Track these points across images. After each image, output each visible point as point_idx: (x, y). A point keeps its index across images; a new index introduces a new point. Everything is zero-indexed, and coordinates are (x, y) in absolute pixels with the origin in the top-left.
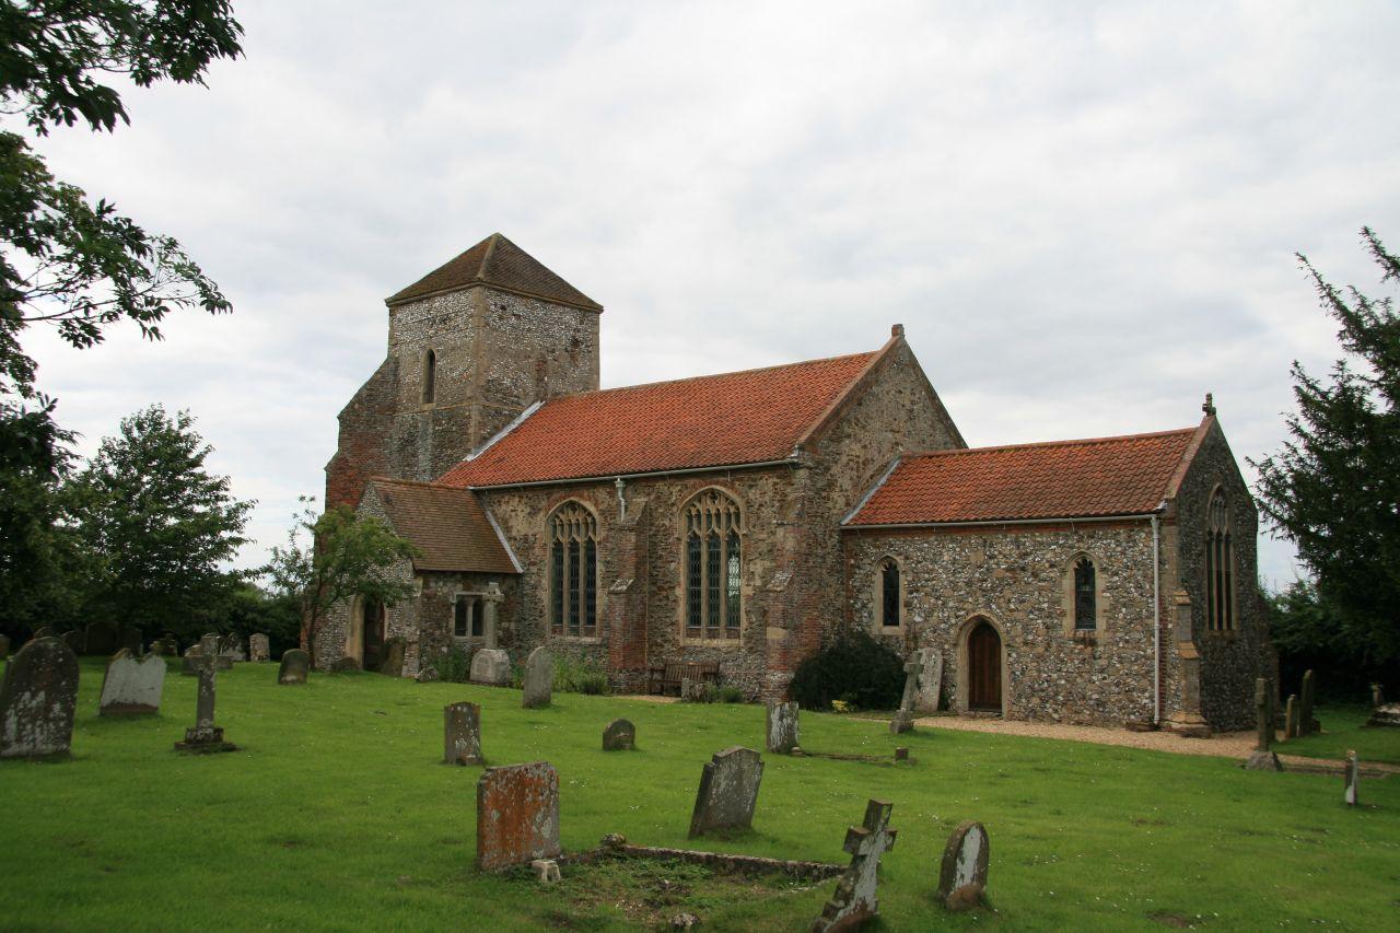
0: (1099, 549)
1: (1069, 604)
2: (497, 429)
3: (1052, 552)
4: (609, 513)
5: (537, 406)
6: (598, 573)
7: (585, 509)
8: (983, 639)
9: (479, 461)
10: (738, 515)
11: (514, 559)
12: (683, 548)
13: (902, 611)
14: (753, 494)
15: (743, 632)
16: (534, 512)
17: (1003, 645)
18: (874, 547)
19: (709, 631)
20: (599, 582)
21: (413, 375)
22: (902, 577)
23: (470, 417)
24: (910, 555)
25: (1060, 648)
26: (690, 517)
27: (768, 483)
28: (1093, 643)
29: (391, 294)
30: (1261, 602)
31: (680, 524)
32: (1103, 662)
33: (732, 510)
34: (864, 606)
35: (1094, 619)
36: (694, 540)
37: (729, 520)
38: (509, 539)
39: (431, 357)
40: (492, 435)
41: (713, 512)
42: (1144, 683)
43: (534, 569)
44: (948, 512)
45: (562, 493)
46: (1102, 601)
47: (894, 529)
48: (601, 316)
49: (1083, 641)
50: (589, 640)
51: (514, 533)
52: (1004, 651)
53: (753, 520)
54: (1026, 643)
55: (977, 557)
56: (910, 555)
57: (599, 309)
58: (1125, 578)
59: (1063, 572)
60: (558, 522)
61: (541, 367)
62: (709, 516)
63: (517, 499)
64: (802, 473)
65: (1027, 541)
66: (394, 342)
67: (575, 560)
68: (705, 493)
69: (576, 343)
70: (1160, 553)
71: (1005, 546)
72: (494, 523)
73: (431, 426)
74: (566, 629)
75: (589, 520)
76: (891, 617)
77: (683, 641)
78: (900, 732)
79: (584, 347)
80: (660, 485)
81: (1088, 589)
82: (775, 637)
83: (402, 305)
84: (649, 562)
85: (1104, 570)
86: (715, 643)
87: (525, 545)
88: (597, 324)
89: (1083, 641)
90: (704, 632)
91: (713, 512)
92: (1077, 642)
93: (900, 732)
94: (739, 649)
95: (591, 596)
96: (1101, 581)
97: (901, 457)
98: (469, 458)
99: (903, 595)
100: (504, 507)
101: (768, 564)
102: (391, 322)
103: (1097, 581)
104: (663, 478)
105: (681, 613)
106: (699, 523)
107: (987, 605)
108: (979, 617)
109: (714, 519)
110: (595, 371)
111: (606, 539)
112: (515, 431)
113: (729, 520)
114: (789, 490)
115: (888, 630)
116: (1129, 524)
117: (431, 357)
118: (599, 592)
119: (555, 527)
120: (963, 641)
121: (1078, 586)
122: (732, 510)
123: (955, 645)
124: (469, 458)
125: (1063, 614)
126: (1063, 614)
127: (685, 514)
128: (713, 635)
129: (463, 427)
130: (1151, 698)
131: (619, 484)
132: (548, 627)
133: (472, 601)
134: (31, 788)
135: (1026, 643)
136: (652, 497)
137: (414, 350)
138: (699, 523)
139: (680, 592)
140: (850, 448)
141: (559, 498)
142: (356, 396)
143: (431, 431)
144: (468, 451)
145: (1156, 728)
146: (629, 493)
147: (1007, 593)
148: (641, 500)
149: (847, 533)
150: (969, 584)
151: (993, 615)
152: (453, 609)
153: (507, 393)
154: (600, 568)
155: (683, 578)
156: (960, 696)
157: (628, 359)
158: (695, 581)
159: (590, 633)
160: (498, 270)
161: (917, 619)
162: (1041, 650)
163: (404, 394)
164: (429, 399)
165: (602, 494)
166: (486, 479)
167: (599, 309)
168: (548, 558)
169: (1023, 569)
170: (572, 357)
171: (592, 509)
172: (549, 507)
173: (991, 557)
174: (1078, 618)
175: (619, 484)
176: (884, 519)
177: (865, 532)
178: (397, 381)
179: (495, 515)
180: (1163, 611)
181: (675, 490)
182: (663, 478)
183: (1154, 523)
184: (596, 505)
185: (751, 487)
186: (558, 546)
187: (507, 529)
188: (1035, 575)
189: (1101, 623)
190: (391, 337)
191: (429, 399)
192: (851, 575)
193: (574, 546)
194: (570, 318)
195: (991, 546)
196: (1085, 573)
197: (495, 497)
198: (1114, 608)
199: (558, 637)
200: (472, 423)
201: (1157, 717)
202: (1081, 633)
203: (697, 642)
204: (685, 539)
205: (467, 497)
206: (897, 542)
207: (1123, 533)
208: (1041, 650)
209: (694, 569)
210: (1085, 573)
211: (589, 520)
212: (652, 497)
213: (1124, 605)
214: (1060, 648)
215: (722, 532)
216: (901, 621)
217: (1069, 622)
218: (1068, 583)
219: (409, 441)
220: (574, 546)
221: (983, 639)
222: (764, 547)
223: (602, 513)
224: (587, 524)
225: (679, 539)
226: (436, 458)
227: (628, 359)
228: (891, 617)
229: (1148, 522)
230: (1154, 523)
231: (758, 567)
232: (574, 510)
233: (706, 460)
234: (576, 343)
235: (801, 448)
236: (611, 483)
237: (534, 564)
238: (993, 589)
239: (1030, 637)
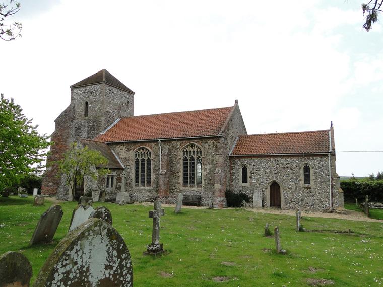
0: (311, 162)
1: (302, 177)
2: (108, 126)
3: (297, 162)
4: (155, 151)
5: (119, 119)
6: (152, 168)
7: (147, 149)
8: (275, 188)
9: (105, 134)
10: (201, 151)
11: (122, 164)
12: (182, 161)
13: (249, 179)
14: (205, 145)
15: (202, 185)
16: (129, 150)
17: (281, 188)
18: (240, 161)
19: (191, 185)
20: (152, 171)
21: (80, 109)
22: (248, 169)
23: (101, 122)
24: (252, 164)
25: (300, 190)
26: (184, 152)
27: (211, 142)
28: (310, 188)
29: (72, 84)
30: (335, 177)
31: (181, 153)
32: (314, 194)
33: (199, 150)
34: (236, 178)
35: (310, 182)
36: (185, 159)
37: (197, 153)
38: (120, 158)
39: (87, 103)
40: (107, 127)
41: (192, 150)
42: (326, 199)
43: (129, 167)
44: (261, 151)
45: (139, 144)
46: (313, 176)
47: (246, 156)
48: (134, 95)
49: (307, 188)
50: (148, 188)
51: (121, 156)
52: (282, 191)
53: (206, 152)
54: (289, 188)
55: (274, 164)
56: (252, 164)
57: (133, 93)
58: (320, 171)
59: (300, 168)
60: (137, 153)
61: (120, 108)
62: (190, 152)
63: (122, 146)
64: (222, 139)
65: (289, 159)
66: (73, 99)
67: (143, 165)
68: (189, 145)
69: (128, 102)
70: (331, 163)
71: (282, 161)
72: (114, 153)
73: (87, 124)
74: (189, 185)
75: (149, 152)
76: (245, 180)
77: (182, 188)
78: (105, 202)
79: (130, 104)
80: (174, 143)
81: (307, 173)
82: (217, 187)
83: (76, 88)
84: (170, 164)
85: (313, 168)
86: (193, 189)
87: (125, 160)
88: (133, 97)
89: (307, 188)
90: (189, 185)
91: (192, 150)
92: (305, 188)
93: (105, 202)
94: (201, 190)
95: (149, 175)
96: (312, 171)
97: (239, 136)
98: (101, 134)
99: (249, 175)
100: (118, 148)
101: (211, 166)
102: (72, 94)
103: (311, 171)
104: (175, 140)
105: (181, 180)
106: (139, 155)
107: (276, 177)
108: (273, 181)
109: (192, 153)
110: (133, 110)
111: (155, 158)
112: (114, 126)
113: (197, 153)
114: (218, 144)
115: (244, 185)
116: (321, 155)
117: (87, 103)
118: (152, 174)
119: (136, 154)
120: (269, 188)
121: (304, 172)
122: (199, 150)
123: (266, 189)
124: (101, 134)
125: (300, 180)
126: (300, 180)
127: (182, 151)
128: (192, 186)
129: (99, 125)
130: (329, 204)
131: (160, 142)
132: (134, 184)
133: (111, 177)
134: (94, 285)
135: (289, 188)
136: (171, 146)
137: (81, 100)
138: (139, 155)
139: (181, 174)
140: (231, 133)
141: (138, 146)
142: (61, 114)
143: (87, 125)
144: (101, 132)
145: (331, 212)
146: (163, 144)
147: (283, 174)
148: (167, 147)
149: (231, 157)
150: (270, 172)
151: (278, 180)
152: (106, 179)
153: (111, 115)
154: (152, 166)
155: (182, 170)
156: (268, 203)
157: (141, 108)
158: (185, 170)
159: (148, 186)
160: (103, 79)
161: (254, 181)
162: (294, 190)
163: (77, 115)
164: (86, 115)
165: (153, 145)
166: (111, 140)
167: (133, 93)
168: (134, 164)
169: (288, 167)
170: (127, 106)
171: (150, 149)
172: (134, 148)
173: (277, 164)
174: (305, 182)
175: (160, 142)
176: (242, 153)
177: (237, 157)
178: (74, 110)
179: (114, 151)
180: (332, 180)
181: (179, 144)
182: (175, 140)
183: (329, 155)
184: (151, 148)
185: (205, 143)
186: (137, 161)
187: (119, 155)
188: (291, 169)
189: (312, 183)
190: (72, 97)
191: (86, 115)
192: (232, 169)
193: (143, 160)
194: (127, 95)
195: (277, 161)
196: (307, 169)
197: (115, 146)
198: (316, 179)
199: (137, 188)
200: (102, 124)
201: (331, 209)
202: (306, 185)
203: (186, 188)
204: (182, 158)
205: (105, 146)
206: (247, 160)
207: (319, 158)
208: (294, 190)
209: (185, 167)
210: (307, 169)
211: (149, 152)
212: (171, 146)
213: (320, 178)
214: (300, 190)
215: (146, 159)
216: (248, 182)
217: (302, 182)
218: (302, 171)
219: (79, 128)
220: (143, 160)
221: (275, 188)
222: (209, 161)
223: (153, 150)
224: (147, 154)
225: (180, 158)
226: (89, 134)
227: (141, 108)
228: (245, 180)
229: (327, 155)
230: (329, 155)
231: (208, 167)
232: (143, 150)
233: (188, 135)
234: (128, 102)
235: (223, 132)
236: (157, 142)
237: (129, 165)
238: (278, 173)
239: (290, 187)
